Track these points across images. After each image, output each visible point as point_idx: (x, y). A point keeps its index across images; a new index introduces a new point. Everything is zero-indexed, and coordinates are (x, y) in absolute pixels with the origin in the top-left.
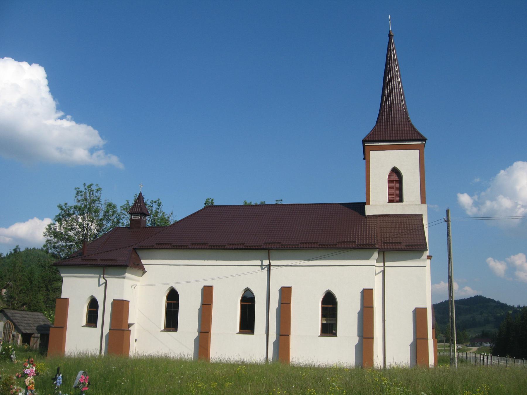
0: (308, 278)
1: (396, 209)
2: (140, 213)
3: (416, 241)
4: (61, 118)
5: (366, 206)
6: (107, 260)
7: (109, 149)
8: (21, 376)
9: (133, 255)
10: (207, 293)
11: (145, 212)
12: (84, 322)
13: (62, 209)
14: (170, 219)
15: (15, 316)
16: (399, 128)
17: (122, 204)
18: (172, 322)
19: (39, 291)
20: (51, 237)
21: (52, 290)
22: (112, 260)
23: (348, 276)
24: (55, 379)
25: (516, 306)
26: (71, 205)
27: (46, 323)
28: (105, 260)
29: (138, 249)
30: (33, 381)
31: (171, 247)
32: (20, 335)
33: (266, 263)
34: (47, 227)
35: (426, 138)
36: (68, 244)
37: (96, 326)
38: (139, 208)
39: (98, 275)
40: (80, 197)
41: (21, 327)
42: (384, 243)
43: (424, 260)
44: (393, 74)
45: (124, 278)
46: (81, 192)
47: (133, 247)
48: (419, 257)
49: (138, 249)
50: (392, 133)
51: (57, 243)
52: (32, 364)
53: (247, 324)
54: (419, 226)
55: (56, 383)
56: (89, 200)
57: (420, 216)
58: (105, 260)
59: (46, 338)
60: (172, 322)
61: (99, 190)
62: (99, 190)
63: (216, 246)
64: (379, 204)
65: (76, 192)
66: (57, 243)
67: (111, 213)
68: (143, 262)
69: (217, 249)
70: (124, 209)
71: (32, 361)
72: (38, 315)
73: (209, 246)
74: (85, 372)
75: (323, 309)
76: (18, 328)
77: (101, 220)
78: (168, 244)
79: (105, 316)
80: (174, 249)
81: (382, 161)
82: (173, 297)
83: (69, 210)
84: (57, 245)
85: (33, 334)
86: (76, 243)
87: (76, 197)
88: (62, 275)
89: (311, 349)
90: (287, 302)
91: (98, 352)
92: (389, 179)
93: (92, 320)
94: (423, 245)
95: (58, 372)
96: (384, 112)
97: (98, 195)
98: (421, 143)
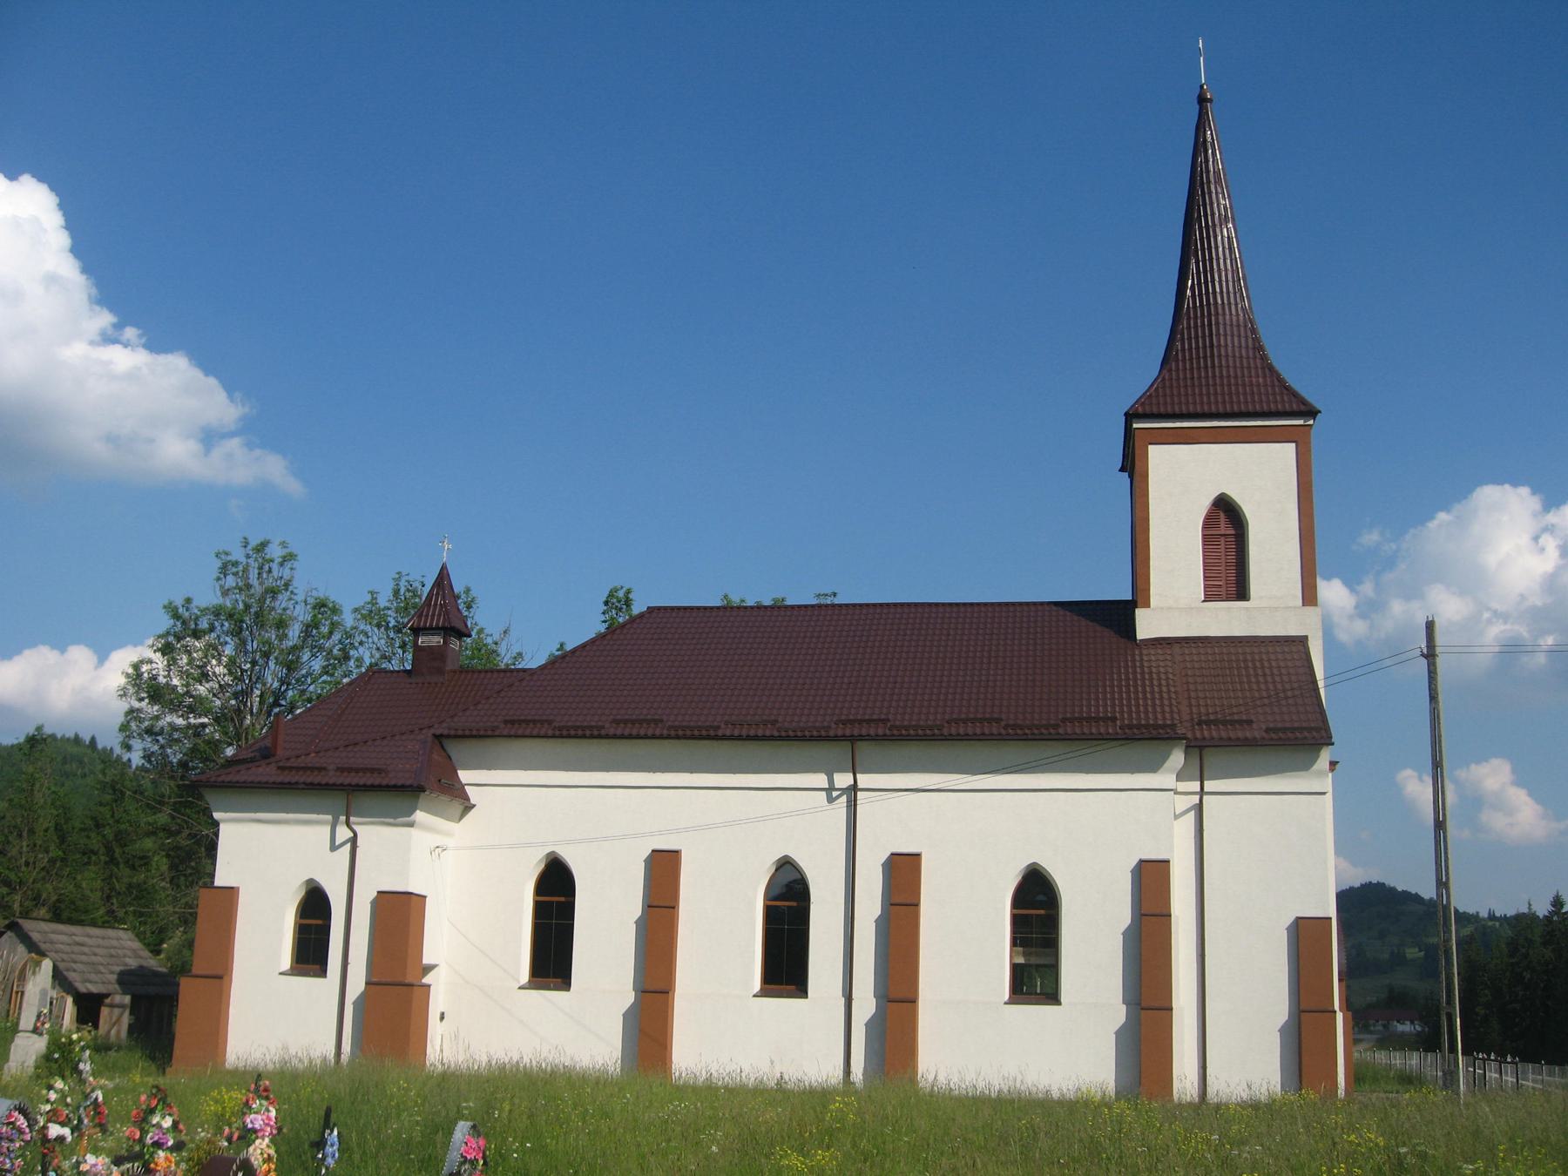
0: (969, 827)
1: (1226, 620)
2: (444, 629)
3: (1286, 717)
4: (108, 339)
5: (1137, 611)
6: (357, 771)
7: (256, 432)
8: (239, 1138)
9: (435, 756)
10: (663, 871)
11: (459, 626)
12: (286, 961)
13: (176, 616)
14: (502, 650)
15: (52, 942)
16: (1236, 377)
17: (359, 603)
18: (552, 960)
19: (88, 863)
20: (141, 700)
21: (127, 862)
22: (372, 770)
23: (1092, 823)
24: (320, 1144)
25: (1484, 914)
26: (203, 605)
27: (145, 964)
28: (350, 770)
29: (448, 736)
30: (272, 1152)
31: (550, 733)
32: (70, 1000)
33: (843, 780)
34: (130, 671)
35: (1318, 406)
36: (192, 721)
37: (322, 972)
38: (438, 614)
39: (329, 817)
40: (231, 581)
41: (71, 976)
42: (1200, 723)
43: (1321, 774)
44: (1213, 214)
45: (411, 825)
46: (236, 564)
47: (432, 731)
48: (1306, 766)
49: (448, 736)
50: (1216, 394)
51: (157, 718)
52: (267, 1098)
53: (785, 967)
54: (1301, 671)
55: (324, 1159)
56: (258, 589)
57: (1303, 640)
58: (350, 770)
59: (161, 1010)
60: (552, 960)
61: (288, 558)
62: (288, 558)
63: (692, 729)
64: (1176, 606)
65: (219, 564)
66: (157, 718)
67: (325, 630)
68: (464, 776)
69: (693, 737)
70: (364, 617)
71: (266, 1090)
72: (118, 939)
73: (670, 728)
74: (474, 1127)
75: (1017, 921)
76: (66, 979)
77: (294, 649)
78: (542, 722)
79: (353, 941)
80: (561, 737)
81: (1185, 476)
82: (556, 886)
83: (197, 618)
84: (161, 723)
85: (107, 996)
86: (217, 720)
87: (219, 579)
88: (216, 815)
89: (978, 1040)
90: (1157, 911)
91: (840, 1073)
92: (1208, 529)
93: (311, 952)
94: (1318, 730)
95: (327, 1124)
96: (1189, 328)
97: (286, 573)
98: (1301, 422)
